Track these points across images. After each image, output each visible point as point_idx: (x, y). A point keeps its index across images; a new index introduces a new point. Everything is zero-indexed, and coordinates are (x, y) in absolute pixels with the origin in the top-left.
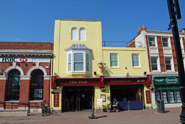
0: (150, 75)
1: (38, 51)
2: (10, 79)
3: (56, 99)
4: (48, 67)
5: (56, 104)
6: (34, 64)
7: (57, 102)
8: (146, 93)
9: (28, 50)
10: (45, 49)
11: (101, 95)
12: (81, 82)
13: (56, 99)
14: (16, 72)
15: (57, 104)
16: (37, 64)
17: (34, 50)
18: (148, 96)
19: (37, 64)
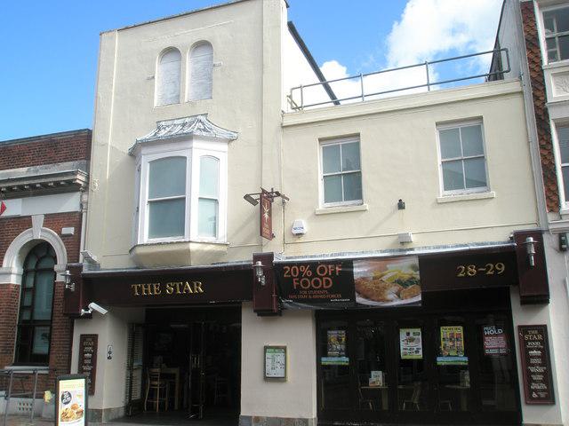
0: (531, 233)
1: (43, 170)
2: (30, 283)
3: (533, 361)
4: (71, 231)
5: (536, 391)
6: (24, 222)
7: (540, 377)
8: (82, 347)
9: (12, 170)
10: (66, 160)
11: (266, 348)
12: (175, 287)
13: (86, 362)
14: (48, 253)
15: (543, 391)
16: (38, 222)
17: (32, 168)
18: (89, 362)
19: (38, 222)
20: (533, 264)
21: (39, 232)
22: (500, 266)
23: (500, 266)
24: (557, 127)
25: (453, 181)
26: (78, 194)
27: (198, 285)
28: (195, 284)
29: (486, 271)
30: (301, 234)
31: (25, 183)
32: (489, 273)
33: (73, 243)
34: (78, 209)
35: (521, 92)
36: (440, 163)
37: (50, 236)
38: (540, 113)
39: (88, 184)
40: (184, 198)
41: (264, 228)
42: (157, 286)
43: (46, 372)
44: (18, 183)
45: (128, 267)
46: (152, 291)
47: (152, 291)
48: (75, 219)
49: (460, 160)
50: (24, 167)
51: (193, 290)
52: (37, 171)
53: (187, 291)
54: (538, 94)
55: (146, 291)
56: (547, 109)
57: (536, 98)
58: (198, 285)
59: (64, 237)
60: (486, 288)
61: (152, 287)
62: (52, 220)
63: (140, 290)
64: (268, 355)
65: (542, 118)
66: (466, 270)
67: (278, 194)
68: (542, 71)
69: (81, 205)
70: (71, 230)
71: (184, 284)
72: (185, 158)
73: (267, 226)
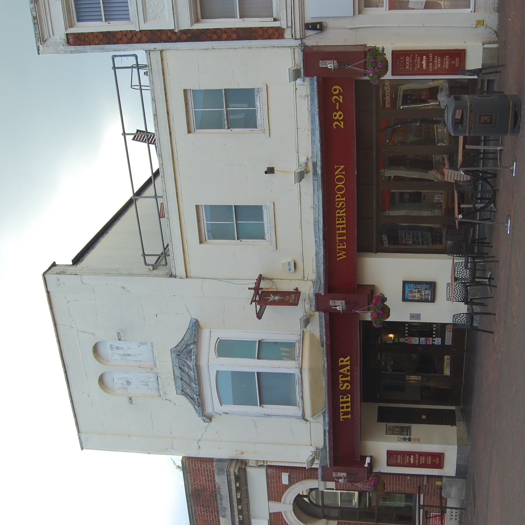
16: (276, 507)
19: (276, 507)
20: (446, 357)
21: (286, 507)
22: (335, 90)
23: (335, 90)
24: (197, 21)
25: (249, 121)
26: (249, 470)
27: (342, 361)
28: (340, 364)
29: (339, 102)
30: (295, 264)
31: (237, 520)
32: (341, 101)
33: (298, 473)
34: (263, 471)
35: (161, 51)
36: (229, 130)
37: (290, 496)
38: (184, 37)
39: (238, 460)
40: (258, 373)
41: (290, 298)
42: (343, 398)
43: (422, 496)
44: (235, 504)
45: (322, 418)
46: (347, 402)
47: (347, 402)
48: (274, 471)
49: (227, 110)
50: (219, 520)
51: (347, 365)
52: (225, 509)
53: (348, 371)
54: (164, 37)
55: (347, 407)
56: (181, 30)
57: (169, 40)
58: (342, 361)
59: (292, 482)
60: (351, 92)
61: (343, 403)
62: (275, 493)
63: (346, 413)
64: (407, 286)
65: (189, 35)
66: (338, 120)
67: (257, 289)
68: (140, 31)
69: (260, 466)
70: (285, 478)
71: (341, 373)
72: (217, 371)
73: (287, 297)
